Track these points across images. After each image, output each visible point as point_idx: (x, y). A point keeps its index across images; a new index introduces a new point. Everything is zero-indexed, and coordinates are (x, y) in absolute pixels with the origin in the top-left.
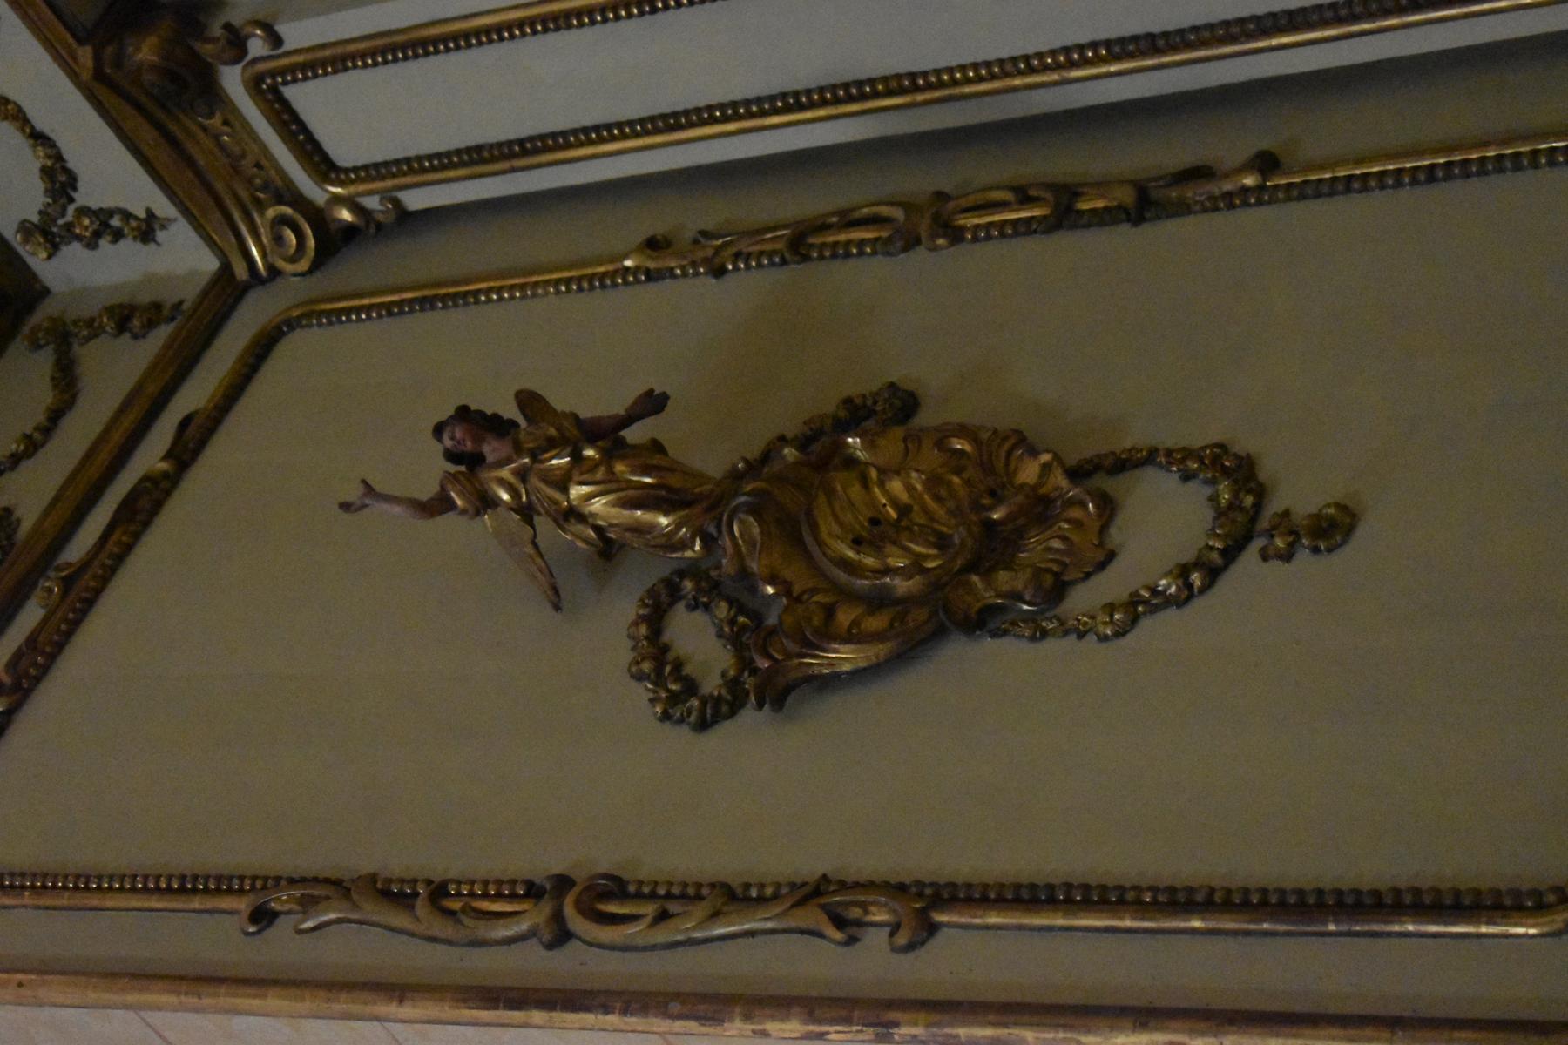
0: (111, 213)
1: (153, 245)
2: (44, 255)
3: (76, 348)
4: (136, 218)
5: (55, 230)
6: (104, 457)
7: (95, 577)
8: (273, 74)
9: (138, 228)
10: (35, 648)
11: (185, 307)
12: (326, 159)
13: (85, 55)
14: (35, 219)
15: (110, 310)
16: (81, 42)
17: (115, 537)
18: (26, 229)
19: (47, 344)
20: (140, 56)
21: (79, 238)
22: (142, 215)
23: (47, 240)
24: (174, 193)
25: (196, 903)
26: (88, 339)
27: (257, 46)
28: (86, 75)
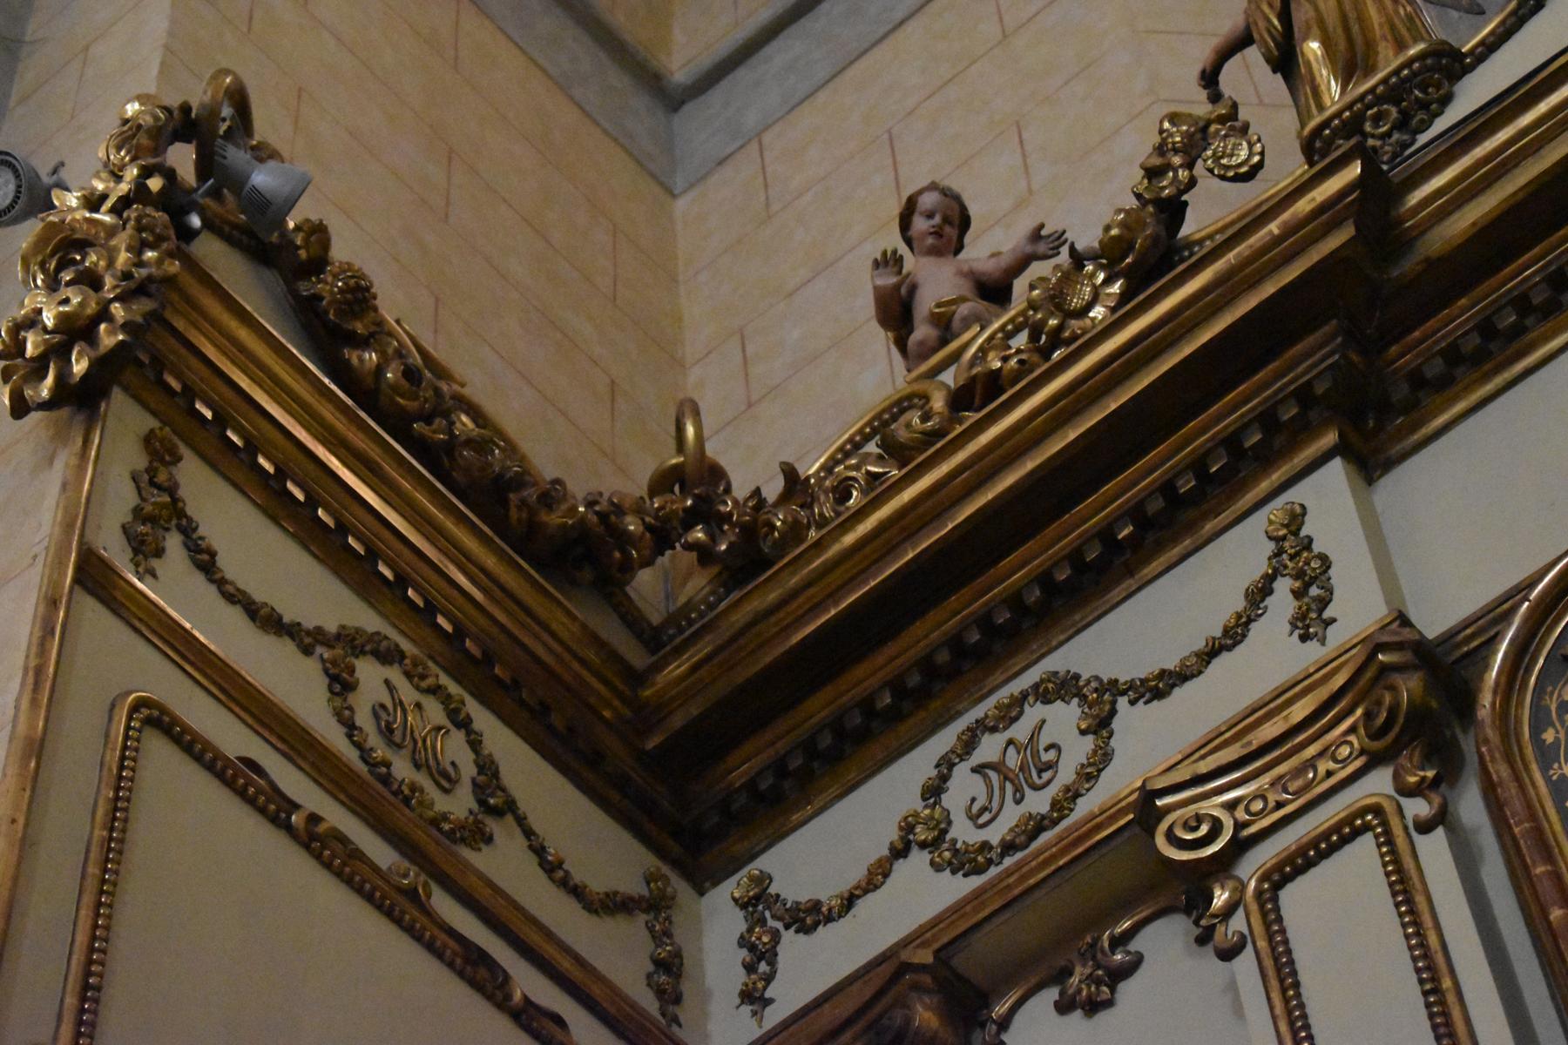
0: (772, 963)
1: (738, 1001)
2: (737, 895)
3: (642, 918)
4: (765, 988)
5: (760, 907)
6: (535, 938)
7: (414, 921)
8: (1384, 823)
9: (755, 989)
10: (350, 856)
11: (675, 1028)
12: (1287, 879)
13: (925, 957)
14: (772, 890)
15: (677, 954)
16: (937, 952)
17: (452, 943)
18: (763, 880)
19: (650, 891)
20: (920, 1008)
21: (750, 930)
22: (767, 995)
23: (750, 899)
24: (794, 1022)
25: (71, 1001)
26: (651, 930)
27: (1418, 808)
28: (905, 956)
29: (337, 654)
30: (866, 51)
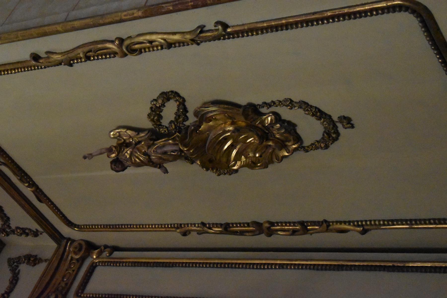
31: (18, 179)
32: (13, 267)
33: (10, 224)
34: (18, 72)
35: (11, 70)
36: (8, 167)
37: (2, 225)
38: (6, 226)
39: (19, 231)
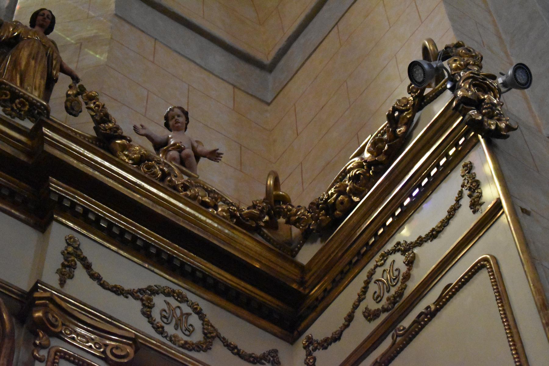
29: (145, 296)
30: (343, 16)
31: (377, 359)
32: (267, 356)
33: (319, 350)
34: (514, 358)
35: (515, 349)
36: (391, 348)
37: (317, 341)
38: (316, 345)
39: (311, 361)
